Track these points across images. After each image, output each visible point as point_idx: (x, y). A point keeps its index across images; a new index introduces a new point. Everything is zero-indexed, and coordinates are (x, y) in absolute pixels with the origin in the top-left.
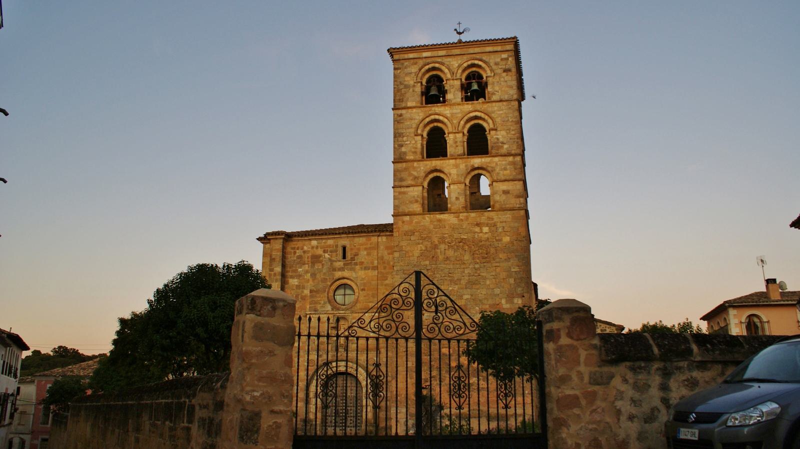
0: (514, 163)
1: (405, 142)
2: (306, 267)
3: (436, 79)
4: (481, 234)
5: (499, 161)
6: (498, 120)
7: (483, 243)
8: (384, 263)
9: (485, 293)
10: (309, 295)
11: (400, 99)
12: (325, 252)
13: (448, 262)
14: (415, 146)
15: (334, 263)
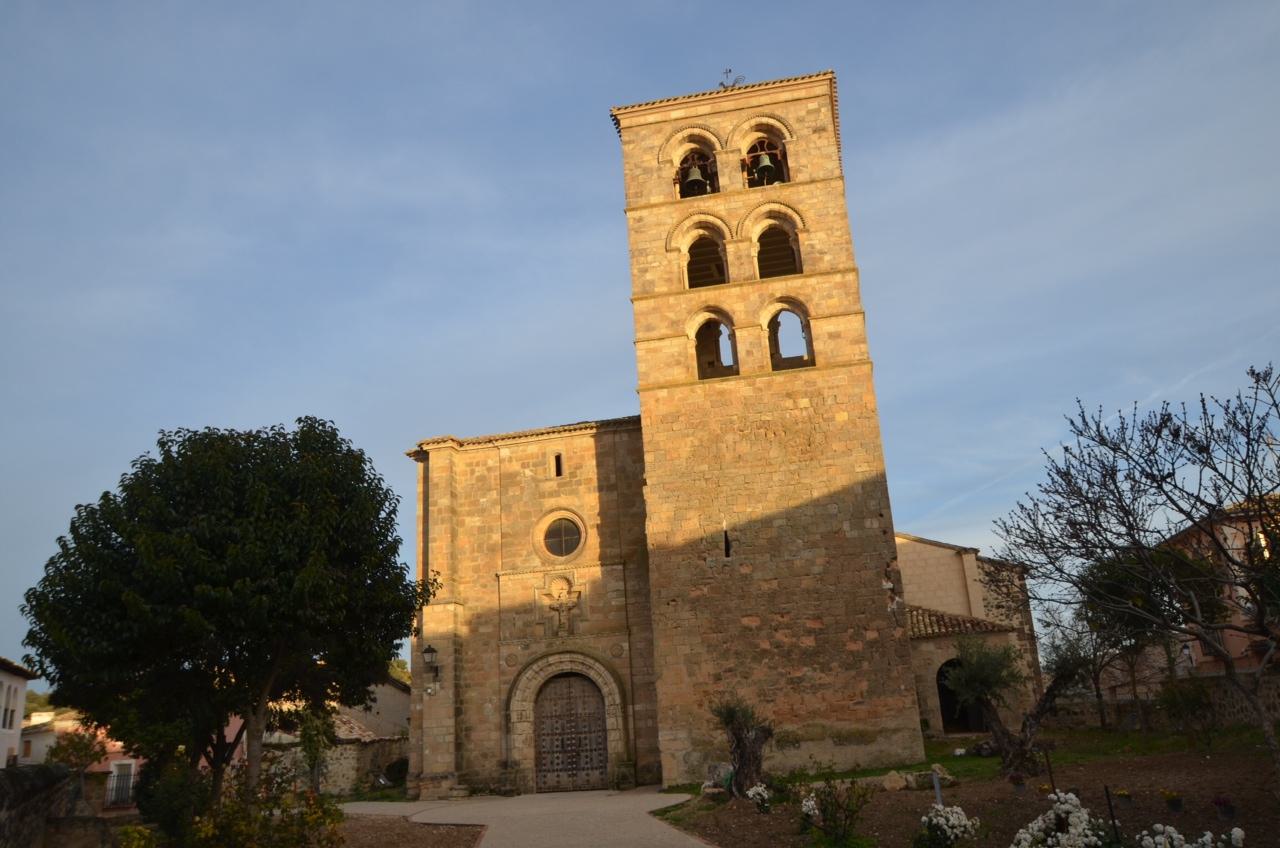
0: (843, 285)
1: (651, 263)
3: (696, 156)
5: (818, 283)
7: (800, 426)
9: (813, 513)
11: (637, 193)
12: (524, 466)
14: (668, 269)
15: (541, 484)
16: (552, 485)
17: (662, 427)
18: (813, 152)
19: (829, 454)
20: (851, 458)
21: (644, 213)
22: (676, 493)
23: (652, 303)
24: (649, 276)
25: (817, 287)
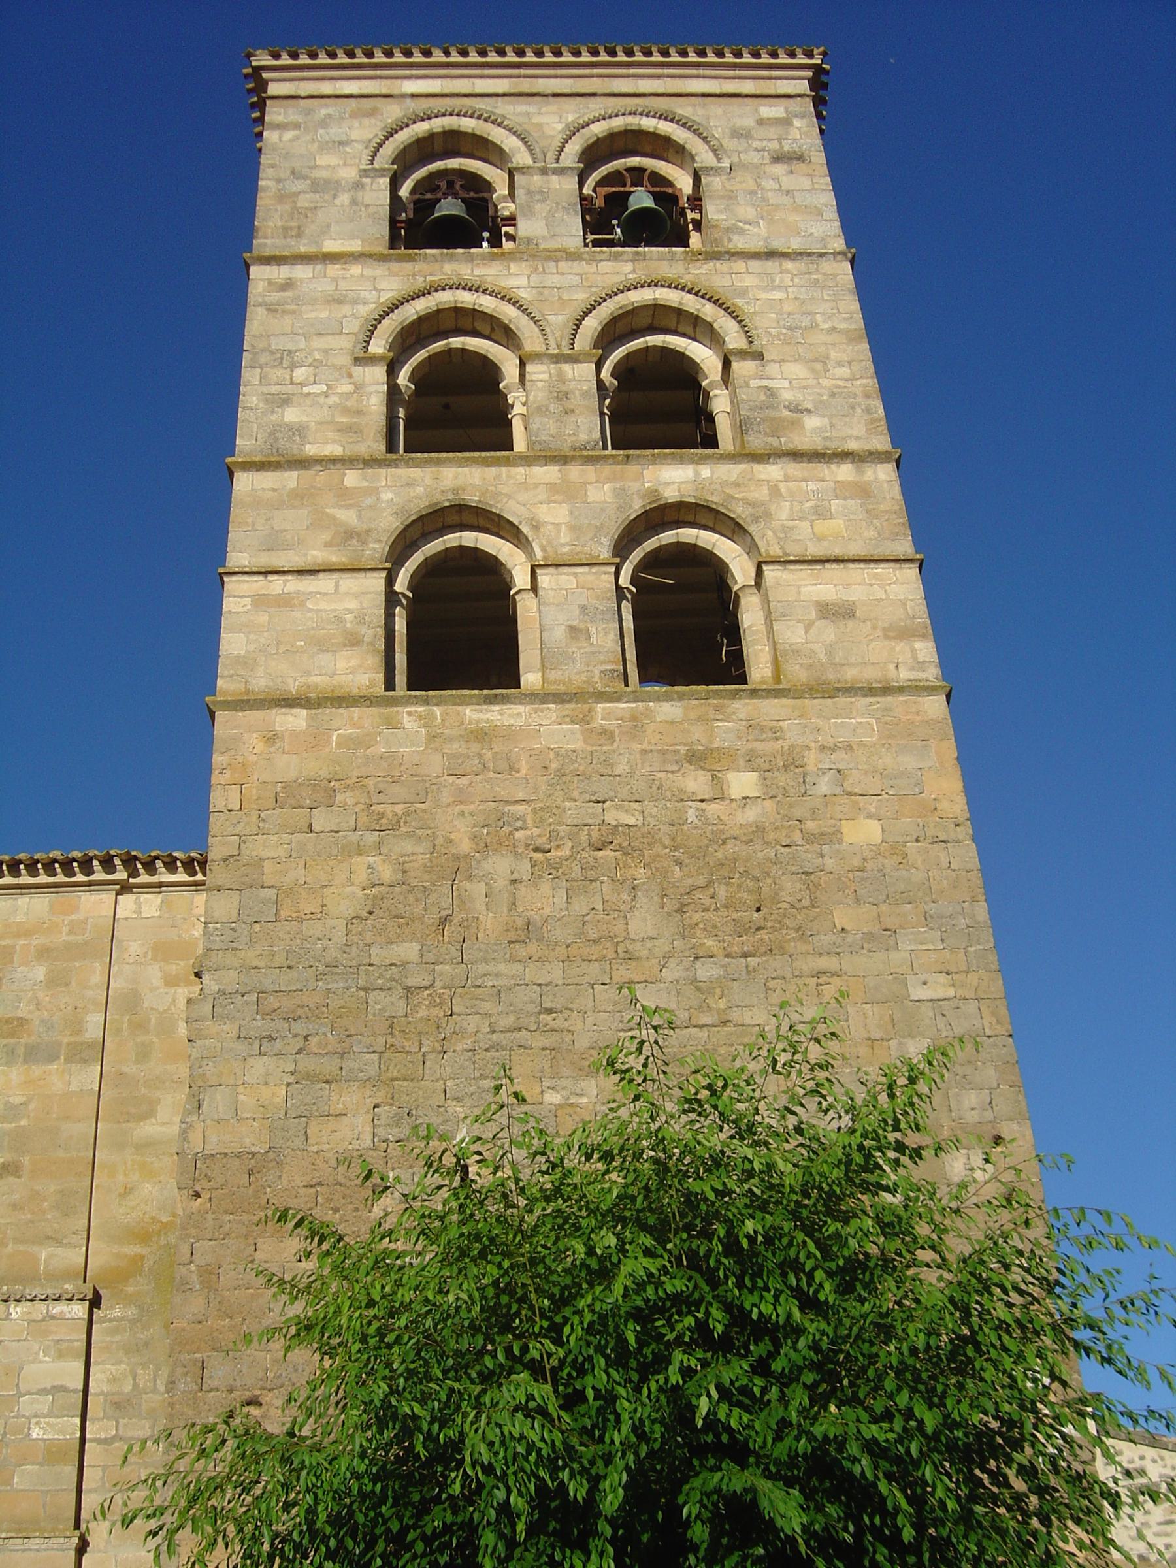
4: (712, 808)
8: (140, 1026)
13: (533, 948)
17: (276, 816)
19: (826, 939)
20: (893, 955)
21: (301, 272)
22: (299, 1028)
23: (291, 479)
24: (291, 415)
25: (783, 487)
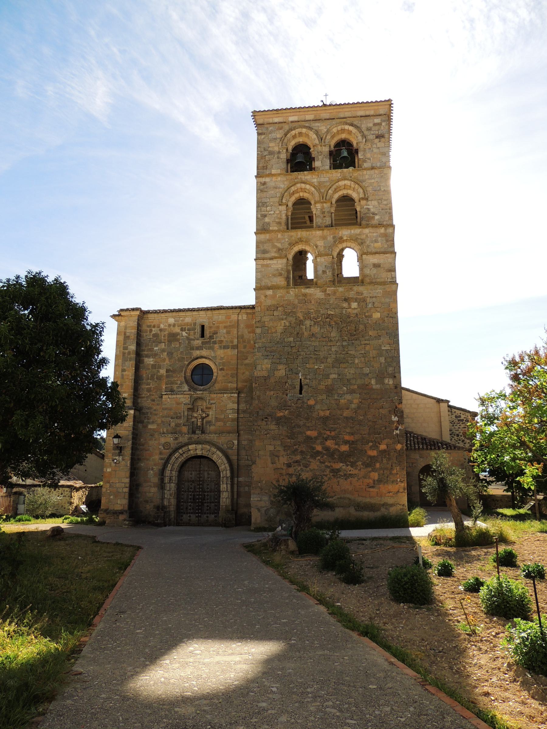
1: (269, 211)
2: (163, 346)
4: (349, 310)
5: (370, 232)
6: (370, 189)
8: (244, 342)
9: (354, 373)
10: (165, 375)
11: (263, 167)
12: (182, 330)
13: (313, 339)
14: (279, 216)
15: (192, 341)
16: (198, 342)
17: (267, 313)
18: (375, 150)
20: (380, 341)
22: (272, 354)
